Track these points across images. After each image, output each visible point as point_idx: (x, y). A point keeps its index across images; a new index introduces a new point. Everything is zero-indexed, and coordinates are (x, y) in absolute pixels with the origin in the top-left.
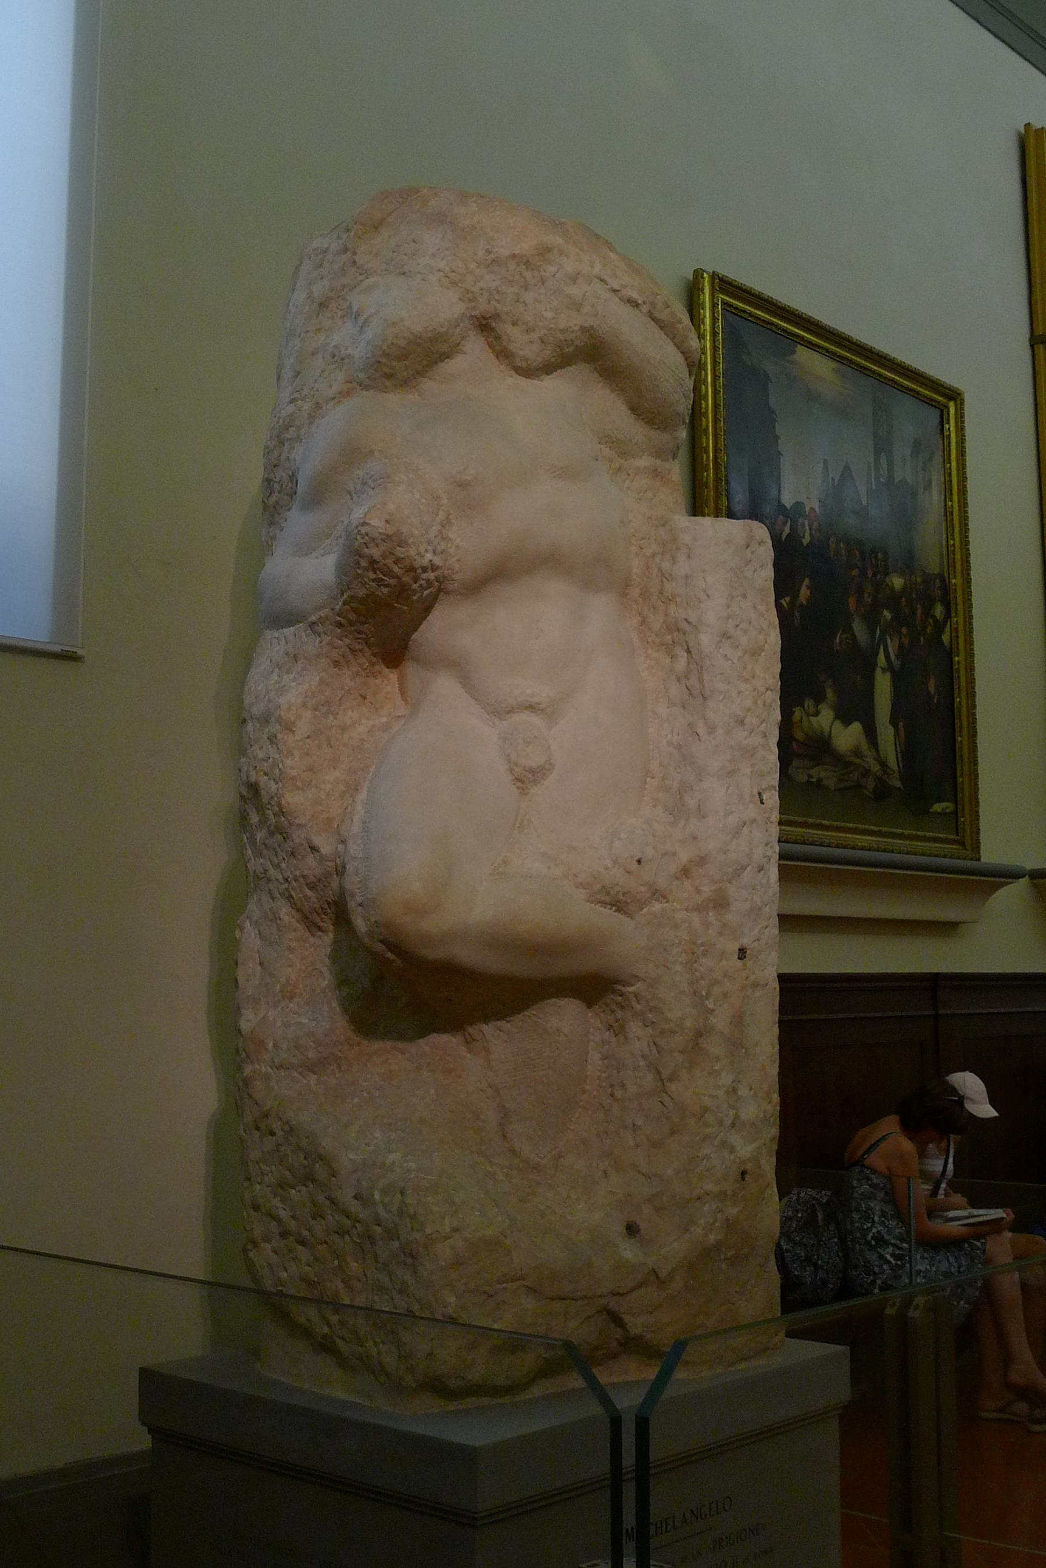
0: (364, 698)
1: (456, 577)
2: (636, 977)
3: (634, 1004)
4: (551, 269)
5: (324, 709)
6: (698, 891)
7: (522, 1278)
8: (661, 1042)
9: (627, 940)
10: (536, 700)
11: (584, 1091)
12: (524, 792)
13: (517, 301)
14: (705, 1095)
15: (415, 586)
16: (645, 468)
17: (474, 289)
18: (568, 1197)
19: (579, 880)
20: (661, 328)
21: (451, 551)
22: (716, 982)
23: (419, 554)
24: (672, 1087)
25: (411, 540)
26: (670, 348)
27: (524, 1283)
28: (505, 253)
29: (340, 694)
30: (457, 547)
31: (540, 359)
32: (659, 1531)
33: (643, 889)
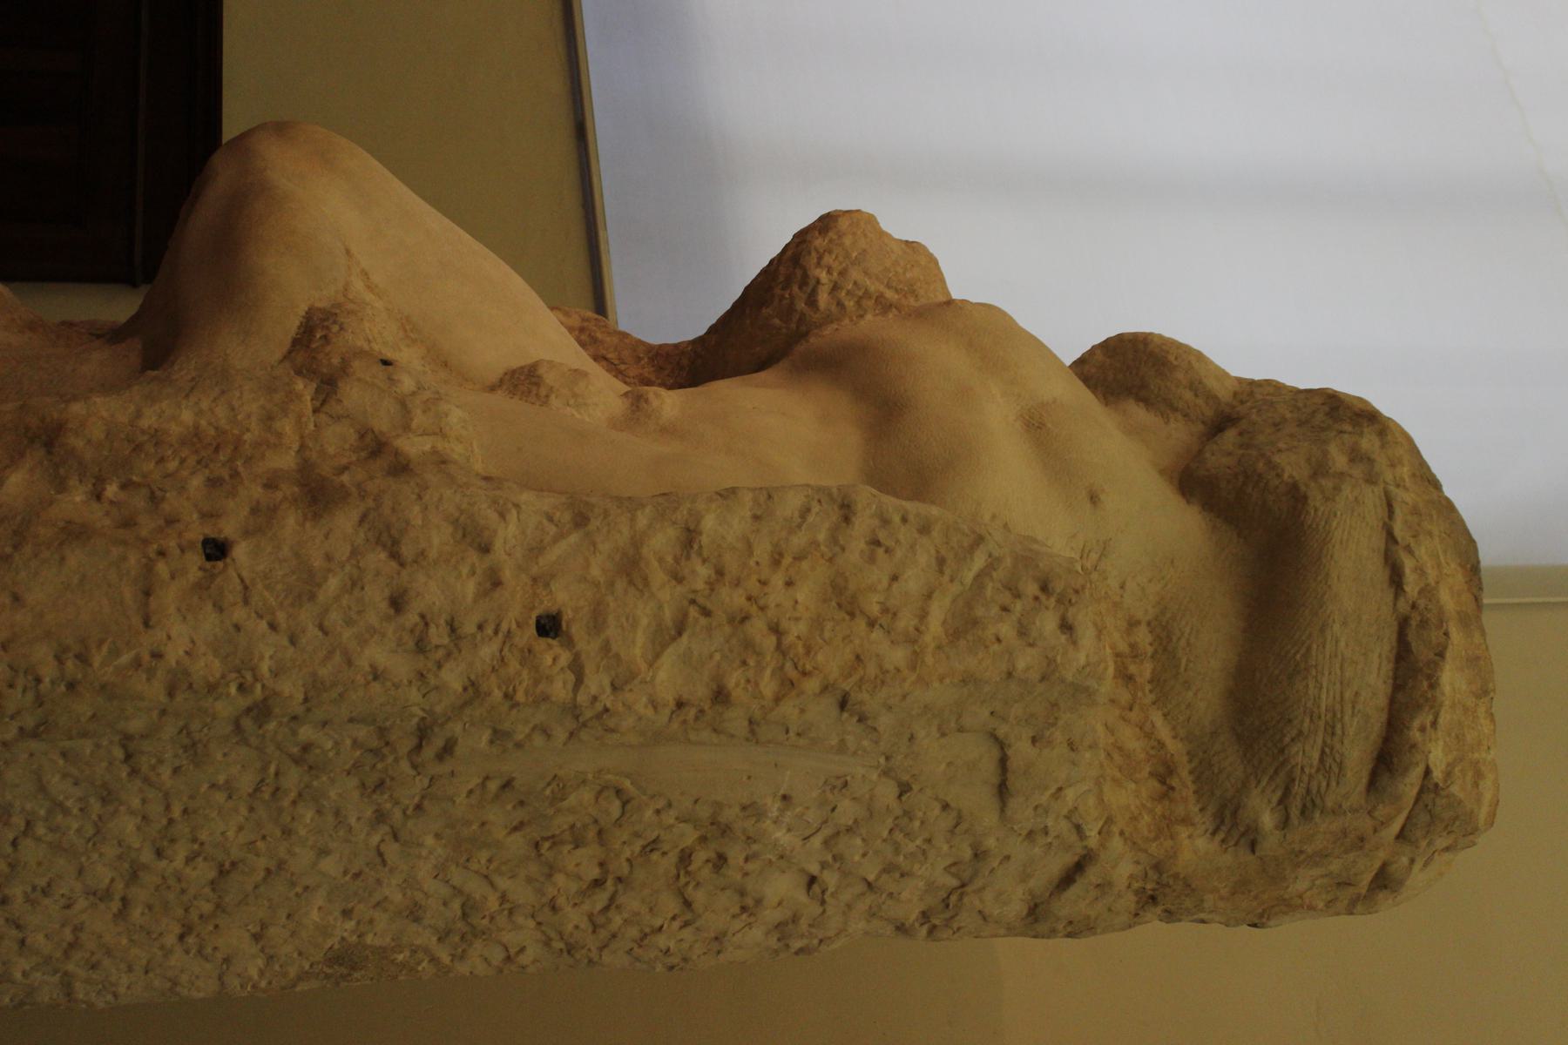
15: (778, 291)
22: (154, 500)
23: (820, 258)
25: (831, 234)
33: (336, 361)
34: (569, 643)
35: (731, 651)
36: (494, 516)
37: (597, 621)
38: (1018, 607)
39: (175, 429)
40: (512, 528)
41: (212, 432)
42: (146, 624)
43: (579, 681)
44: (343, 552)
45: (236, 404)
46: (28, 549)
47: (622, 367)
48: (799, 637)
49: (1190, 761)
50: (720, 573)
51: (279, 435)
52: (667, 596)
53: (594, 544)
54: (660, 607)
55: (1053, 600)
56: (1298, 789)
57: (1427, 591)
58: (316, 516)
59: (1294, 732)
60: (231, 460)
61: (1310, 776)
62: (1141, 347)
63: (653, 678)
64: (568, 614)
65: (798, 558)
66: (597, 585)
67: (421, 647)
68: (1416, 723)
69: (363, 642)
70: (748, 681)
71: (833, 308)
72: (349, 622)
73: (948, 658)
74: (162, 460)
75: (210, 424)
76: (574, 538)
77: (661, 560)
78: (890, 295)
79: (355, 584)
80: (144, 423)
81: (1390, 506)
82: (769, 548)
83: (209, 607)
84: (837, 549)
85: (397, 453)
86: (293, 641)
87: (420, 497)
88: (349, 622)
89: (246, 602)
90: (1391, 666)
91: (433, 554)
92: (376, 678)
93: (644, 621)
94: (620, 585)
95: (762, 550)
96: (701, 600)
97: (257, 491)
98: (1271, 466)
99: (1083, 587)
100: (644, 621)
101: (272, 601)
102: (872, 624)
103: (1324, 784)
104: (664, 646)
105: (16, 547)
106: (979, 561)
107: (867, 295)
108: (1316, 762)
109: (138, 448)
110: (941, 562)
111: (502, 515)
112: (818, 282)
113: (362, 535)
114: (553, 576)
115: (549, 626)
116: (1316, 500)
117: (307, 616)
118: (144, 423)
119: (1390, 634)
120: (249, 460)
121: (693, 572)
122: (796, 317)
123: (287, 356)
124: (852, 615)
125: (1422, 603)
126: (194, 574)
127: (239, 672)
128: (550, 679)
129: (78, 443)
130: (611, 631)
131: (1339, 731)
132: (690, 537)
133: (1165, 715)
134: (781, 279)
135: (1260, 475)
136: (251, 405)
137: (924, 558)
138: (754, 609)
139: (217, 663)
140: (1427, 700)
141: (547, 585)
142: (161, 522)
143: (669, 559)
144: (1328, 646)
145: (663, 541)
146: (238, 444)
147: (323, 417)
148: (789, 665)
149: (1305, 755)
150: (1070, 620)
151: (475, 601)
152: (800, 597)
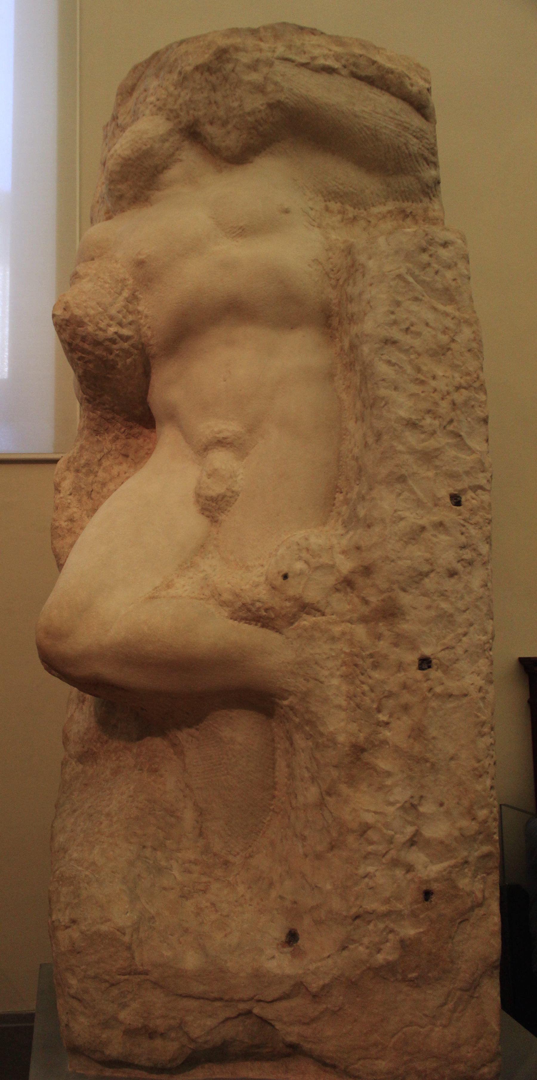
0: (126, 456)
1: (152, 342)
2: (290, 693)
3: (294, 718)
4: (229, 66)
6: (366, 602)
7: (146, 973)
8: (318, 755)
9: (274, 652)
10: (221, 436)
11: (274, 797)
12: (214, 521)
14: (368, 811)
15: (111, 357)
16: (389, 212)
17: (176, 107)
18: (243, 896)
21: (142, 321)
22: (390, 695)
23: (101, 329)
24: (330, 801)
25: (86, 320)
28: (189, 69)
29: (99, 456)
30: (146, 317)
33: (288, 604)
34: (464, 491)
35: (466, 412)
36: (402, 524)
37: (453, 476)
38: (436, 266)
39: (344, 688)
40: (407, 514)
41: (344, 668)
42: (466, 695)
44: (426, 600)
45: (325, 656)
46: (428, 755)
47: (105, 451)
48: (461, 378)
49: (398, 200)
50: (429, 411)
51: (344, 634)
52: (442, 440)
55: (431, 248)
56: (426, 153)
57: (337, 57)
58: (403, 614)
59: (404, 147)
60: (363, 658)
61: (423, 146)
62: (130, 162)
63: (480, 452)
64: (451, 490)
65: (419, 370)
66: (436, 474)
67: (470, 563)
68: (410, 87)
69: (470, 591)
70: (480, 406)
71: (133, 327)
72: (462, 598)
73: (464, 306)
74: (363, 693)
75: (338, 669)
76: (410, 482)
77: (423, 441)
78: (126, 294)
79: (443, 594)
80: (344, 703)
84: (411, 350)
85: (353, 572)
86: (471, 625)
87: (393, 561)
88: (462, 598)
89: (453, 648)
91: (427, 555)
92: (486, 585)
94: (438, 463)
95: (416, 389)
96: (445, 423)
98: (252, 113)
99: (424, 231)
101: (452, 635)
102: (453, 341)
103: (426, 141)
104: (465, 444)
105: (427, 761)
106: (411, 279)
108: (418, 141)
109: (358, 706)
110: (416, 299)
111: (402, 519)
112: (116, 333)
113: (414, 591)
115: (456, 500)
116: (281, 97)
117: (460, 618)
118: (344, 703)
119: (358, 84)
121: (430, 425)
122: (132, 350)
123: (278, 631)
124: (449, 349)
125: (343, 62)
126: (439, 674)
127: (485, 650)
128: (482, 502)
129: (362, 736)
131: (407, 125)
132: (413, 425)
133: (373, 206)
134: (104, 354)
135: (256, 121)
136: (323, 649)
137: (414, 307)
138: (449, 398)
141: (439, 499)
143: (423, 436)
144: (366, 116)
145: (412, 438)
146: (351, 654)
147: (328, 611)
150: (442, 242)
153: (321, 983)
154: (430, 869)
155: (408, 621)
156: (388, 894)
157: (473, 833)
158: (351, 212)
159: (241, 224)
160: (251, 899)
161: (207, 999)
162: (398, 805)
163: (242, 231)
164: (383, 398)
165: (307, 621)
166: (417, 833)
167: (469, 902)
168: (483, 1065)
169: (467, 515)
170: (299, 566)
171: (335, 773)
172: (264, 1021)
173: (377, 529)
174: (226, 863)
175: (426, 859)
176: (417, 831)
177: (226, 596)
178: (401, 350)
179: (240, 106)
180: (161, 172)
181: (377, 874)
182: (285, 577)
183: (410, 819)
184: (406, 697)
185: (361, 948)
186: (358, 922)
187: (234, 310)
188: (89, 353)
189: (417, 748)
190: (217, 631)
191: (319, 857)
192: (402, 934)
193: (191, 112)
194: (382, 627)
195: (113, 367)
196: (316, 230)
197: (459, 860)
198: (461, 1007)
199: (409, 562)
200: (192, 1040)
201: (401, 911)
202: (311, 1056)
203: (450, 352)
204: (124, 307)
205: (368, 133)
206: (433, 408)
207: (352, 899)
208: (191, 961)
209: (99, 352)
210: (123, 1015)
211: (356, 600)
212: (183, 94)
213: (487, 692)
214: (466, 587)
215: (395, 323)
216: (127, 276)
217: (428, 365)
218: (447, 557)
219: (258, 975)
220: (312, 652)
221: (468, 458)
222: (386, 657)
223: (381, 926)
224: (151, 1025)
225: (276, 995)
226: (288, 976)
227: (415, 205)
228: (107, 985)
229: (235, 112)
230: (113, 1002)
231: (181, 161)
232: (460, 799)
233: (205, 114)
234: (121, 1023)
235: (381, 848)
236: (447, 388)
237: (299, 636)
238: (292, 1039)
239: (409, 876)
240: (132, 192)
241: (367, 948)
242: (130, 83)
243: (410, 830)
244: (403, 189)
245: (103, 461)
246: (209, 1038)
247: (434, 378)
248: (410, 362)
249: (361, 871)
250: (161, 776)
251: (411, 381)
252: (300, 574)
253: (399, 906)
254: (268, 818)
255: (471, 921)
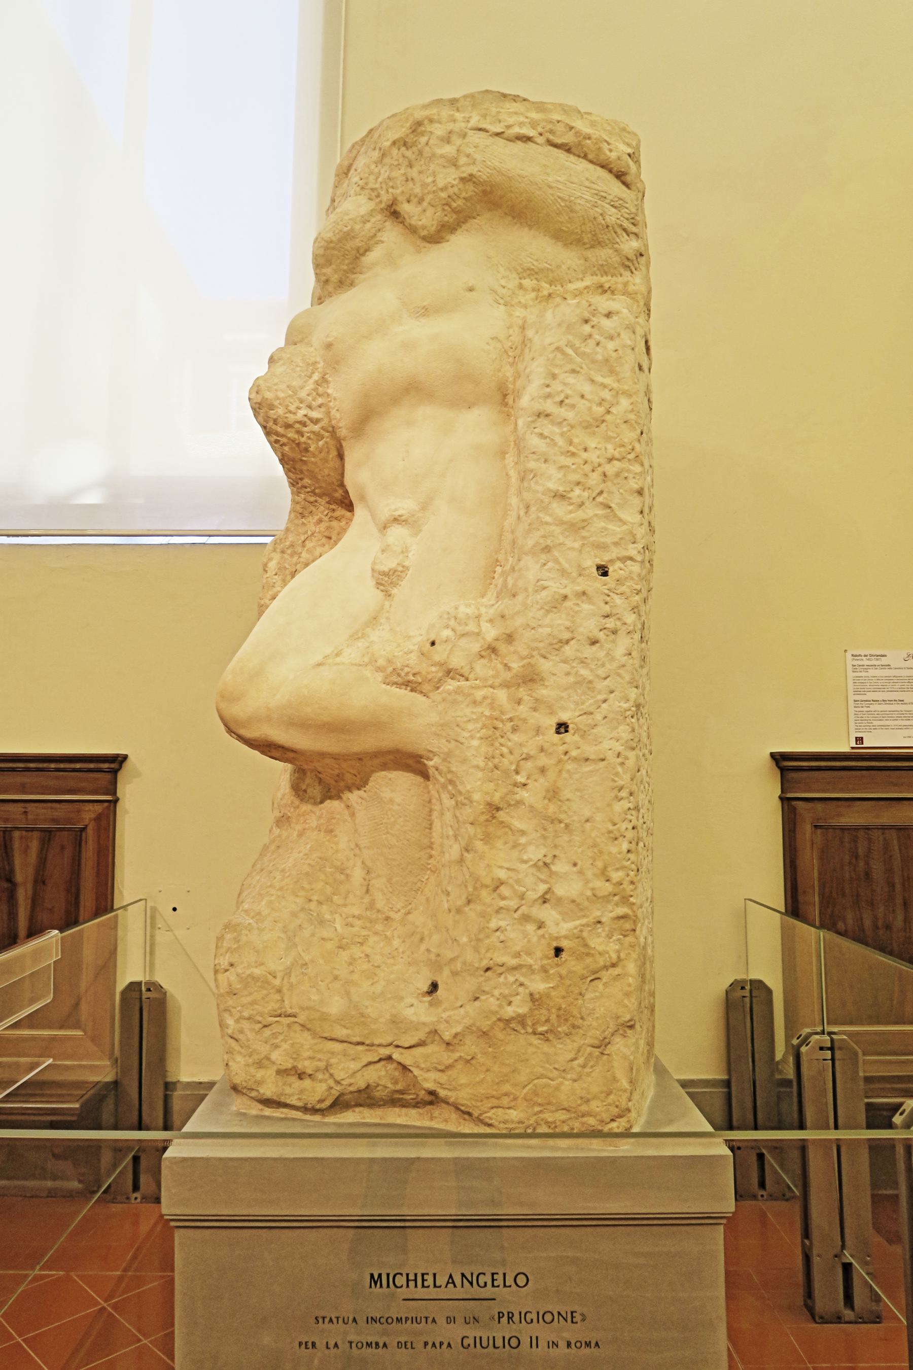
1: (341, 425)
2: (435, 754)
3: (439, 777)
4: (423, 140)
5: (289, 551)
6: (507, 667)
9: (418, 720)
10: (397, 513)
11: (431, 856)
13: (407, 180)
15: (303, 440)
16: (586, 287)
17: (377, 186)
19: (378, 664)
20: (569, 151)
23: (290, 412)
25: (276, 403)
26: (583, 165)
27: (296, 1020)
29: (303, 538)
30: (335, 399)
31: (435, 223)
32: (412, 1284)
33: (434, 669)
34: (612, 561)
36: (544, 593)
37: (603, 547)
38: (597, 337)
39: (483, 749)
43: (631, 559)
44: (565, 667)
45: (466, 719)
46: (562, 816)
47: (309, 533)
50: (578, 483)
51: (485, 698)
52: (590, 511)
53: (560, 544)
54: (596, 515)
55: (594, 319)
56: (626, 224)
59: (601, 218)
60: (502, 721)
62: (332, 245)
65: (571, 443)
67: (614, 632)
68: (608, 153)
69: (613, 659)
71: (323, 409)
72: (603, 665)
77: (571, 512)
78: (316, 377)
80: (482, 764)
81: (480, 130)
82: (563, 457)
83: (594, 731)
84: (565, 423)
86: (612, 692)
87: (533, 628)
88: (603, 665)
89: (592, 713)
90: (571, 156)
91: (568, 624)
93: (603, 524)
94: (584, 533)
95: (568, 461)
96: (594, 495)
97: (523, 710)
100: (603, 524)
102: (608, 412)
104: (615, 516)
106: (570, 351)
107: (315, 390)
110: (573, 371)
111: (545, 588)
112: (306, 416)
114: (579, 566)
115: (603, 571)
118: (482, 764)
120: (502, 713)
121: (579, 496)
122: (323, 432)
124: (603, 421)
125: (540, 130)
126: (576, 738)
130: (608, 540)
131: (604, 194)
132: (562, 497)
134: (296, 436)
135: (449, 197)
137: (571, 379)
139: (622, 728)
140: (596, 143)
142: (543, 754)
143: (571, 508)
144: (560, 187)
145: (560, 509)
146: (491, 718)
147: (472, 676)
148: (630, 457)
149: (613, 216)
150: (606, 312)
151: (593, 604)
152: (593, 445)
153: (454, 1031)
154: (560, 926)
155: (547, 686)
156: (518, 948)
157: (606, 893)
158: (546, 289)
159: (425, 304)
160: (403, 953)
161: (350, 1043)
162: (531, 863)
163: (424, 312)
164: (532, 471)
165: (451, 685)
166: (549, 891)
167: (601, 962)
168: (612, 1120)
169: (612, 584)
170: (447, 633)
171: (471, 830)
172: (405, 1068)
173: (520, 598)
174: (387, 918)
175: (559, 917)
176: (550, 889)
177: (381, 662)
178: (553, 423)
179: (434, 182)
180: (363, 254)
181: (508, 928)
182: (433, 644)
183: (542, 877)
184: (543, 760)
185: (492, 1000)
186: (489, 973)
187: (413, 390)
188: (283, 436)
189: (552, 809)
190: (369, 695)
191: (459, 911)
192: (531, 989)
193: (390, 190)
194: (522, 692)
195: (306, 450)
196: (502, 307)
197: (591, 919)
198: (591, 1064)
199: (549, 630)
200: (338, 1082)
201: (531, 966)
202: (448, 1103)
203: (604, 424)
204: (314, 390)
205: (563, 204)
206: (582, 480)
207: (483, 951)
208: (335, 1006)
209: (291, 434)
210: (274, 1056)
211: (500, 666)
212: (382, 171)
213: (627, 758)
214: (608, 654)
215: (549, 396)
216: (318, 359)
217: (580, 436)
218: (590, 626)
219: (395, 1021)
220: (453, 714)
221: (618, 529)
222: (525, 720)
223: (511, 979)
224: (300, 1066)
225: (412, 1043)
226: (424, 1024)
227: (614, 279)
228: (260, 1026)
229: (429, 188)
230: (266, 1042)
231: (382, 242)
232: (595, 860)
233: (403, 192)
234: (274, 1063)
235: (513, 903)
236: (598, 460)
237: (444, 700)
238: (430, 1086)
239: (541, 932)
240: (336, 276)
241: (498, 999)
242: (346, 163)
243: (543, 887)
244: (600, 262)
245: (307, 542)
246: (352, 1081)
247: (586, 450)
248: (562, 434)
249: (493, 924)
250: (336, 836)
251: (562, 454)
252: (446, 641)
253: (530, 961)
254: (426, 877)
255: (604, 980)
